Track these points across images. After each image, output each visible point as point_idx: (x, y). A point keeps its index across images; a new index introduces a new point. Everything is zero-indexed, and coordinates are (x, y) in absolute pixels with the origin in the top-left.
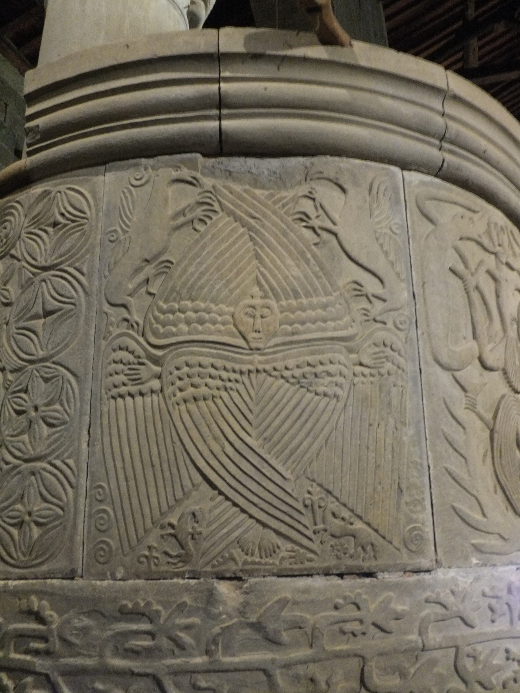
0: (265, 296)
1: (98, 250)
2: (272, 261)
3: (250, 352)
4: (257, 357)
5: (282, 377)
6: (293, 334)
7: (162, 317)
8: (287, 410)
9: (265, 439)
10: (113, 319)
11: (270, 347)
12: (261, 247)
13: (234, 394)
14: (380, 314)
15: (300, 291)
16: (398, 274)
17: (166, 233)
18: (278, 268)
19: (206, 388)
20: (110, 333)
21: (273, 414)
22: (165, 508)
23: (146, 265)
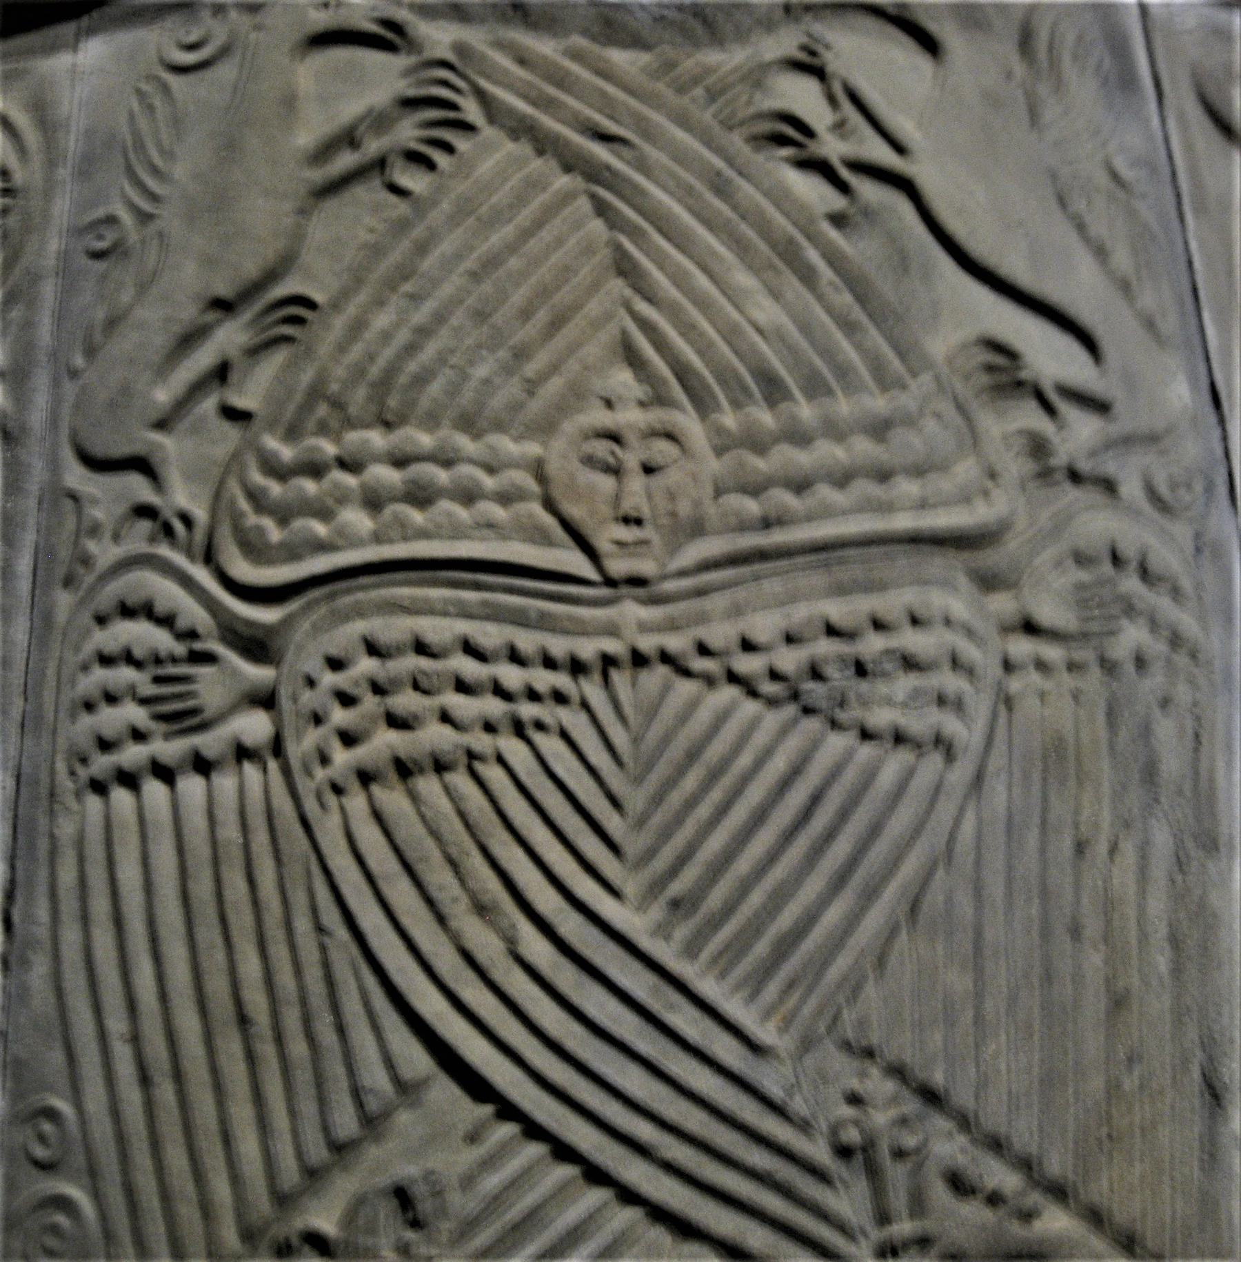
0: (660, 399)
1: (48, 291)
2: (680, 280)
3: (604, 592)
4: (631, 611)
5: (733, 678)
6: (767, 524)
7: (275, 489)
8: (755, 794)
9: (675, 904)
10: (98, 513)
11: (682, 573)
12: (636, 234)
13: (551, 745)
14: (1093, 454)
16: (1150, 324)
17: (288, 206)
18: (703, 304)
19: (447, 731)
20: (86, 561)
21: (704, 811)
22: (290, 1174)
23: (219, 322)
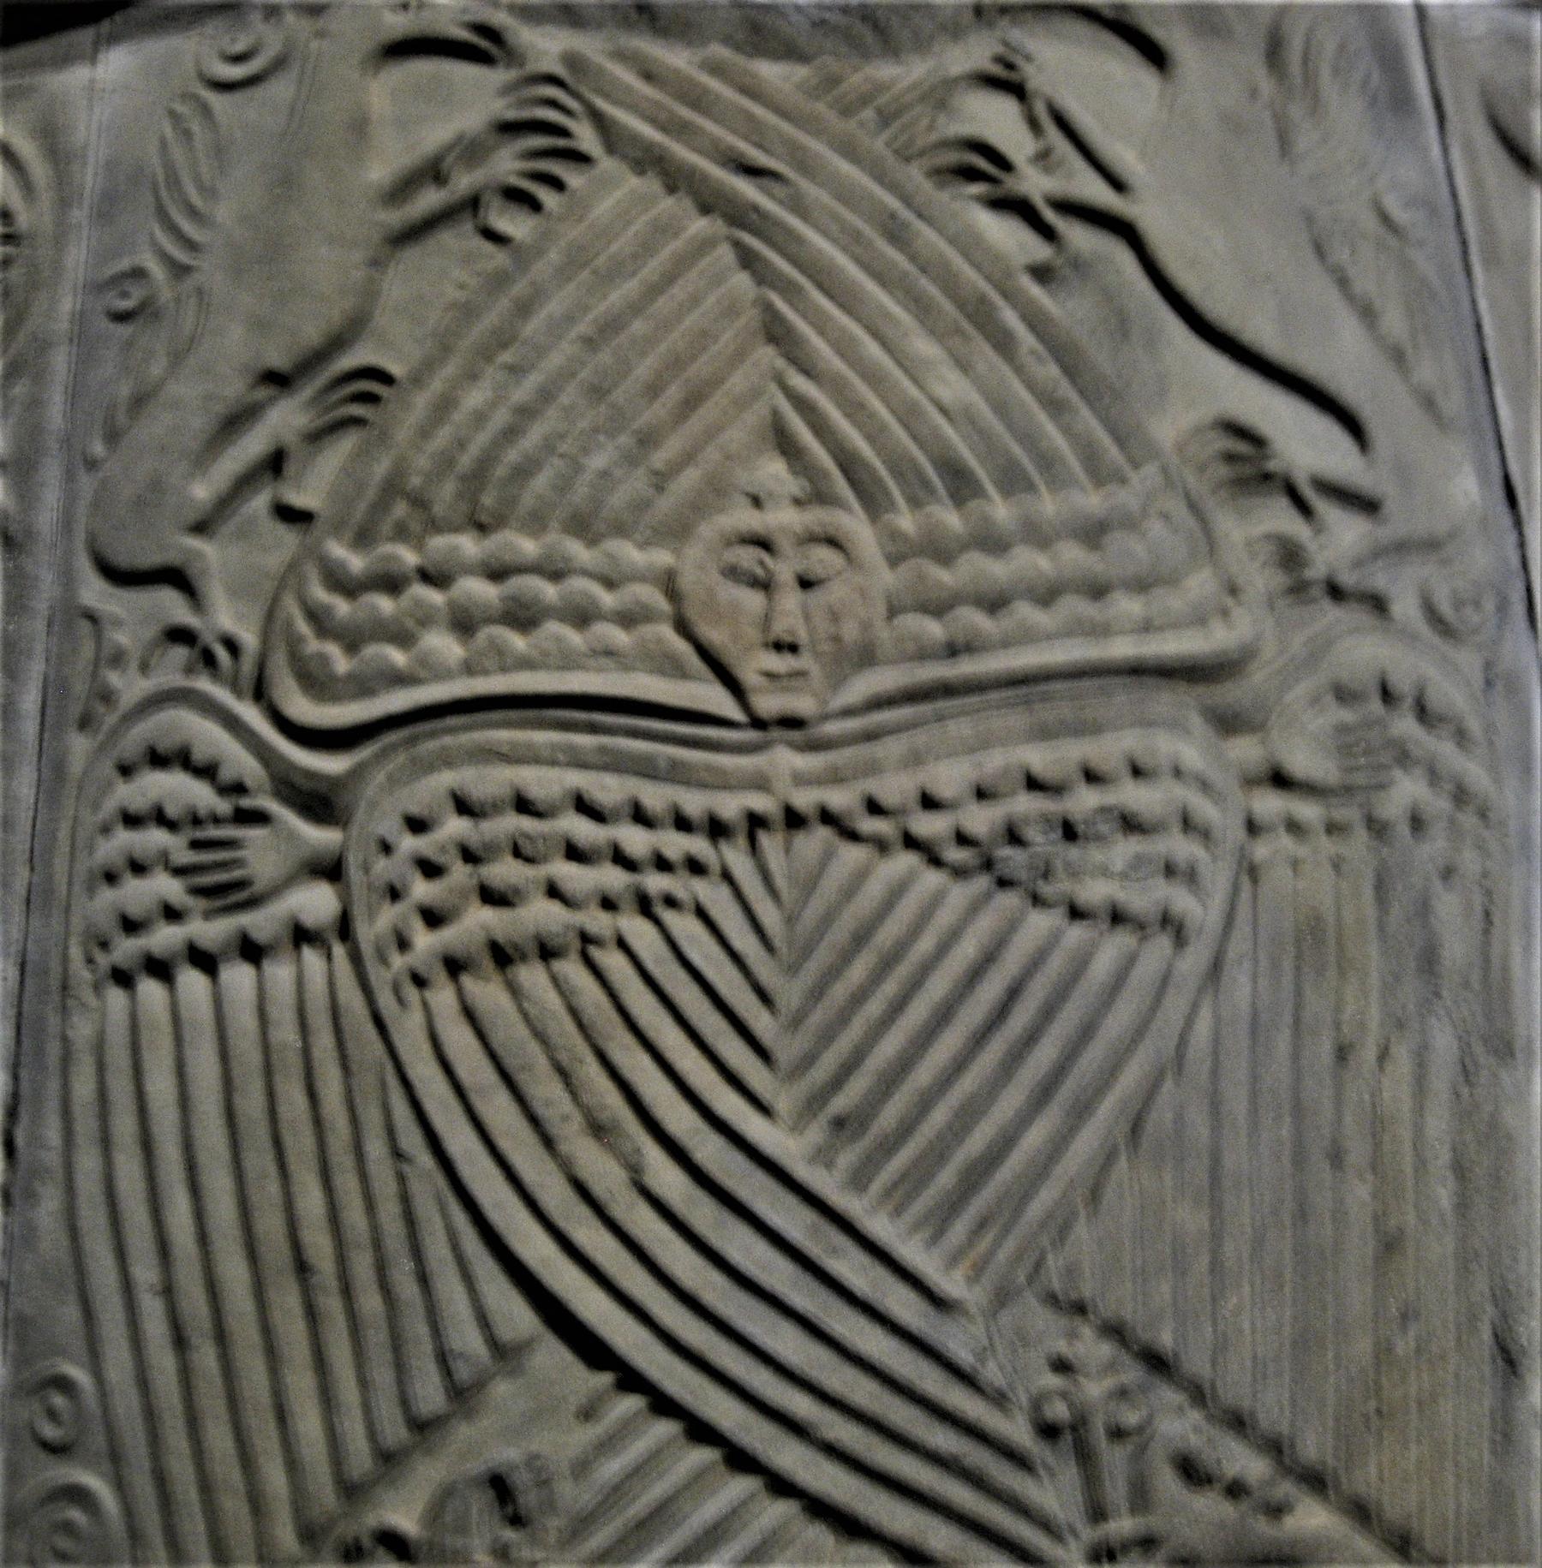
0: (819, 496)
1: (60, 361)
2: (845, 348)
3: (751, 735)
4: (784, 760)
5: (911, 842)
6: (953, 650)
7: (342, 607)
8: (938, 986)
9: (839, 1123)
10: (122, 638)
11: (848, 712)
12: (790, 291)
13: (684, 926)
14: (1358, 564)
15: (981, 473)
16: (1429, 403)
17: (358, 256)
18: (874, 378)
19: (555, 908)
20: (107, 696)
21: (874, 1007)
22: (360, 1458)
23: (272, 401)
